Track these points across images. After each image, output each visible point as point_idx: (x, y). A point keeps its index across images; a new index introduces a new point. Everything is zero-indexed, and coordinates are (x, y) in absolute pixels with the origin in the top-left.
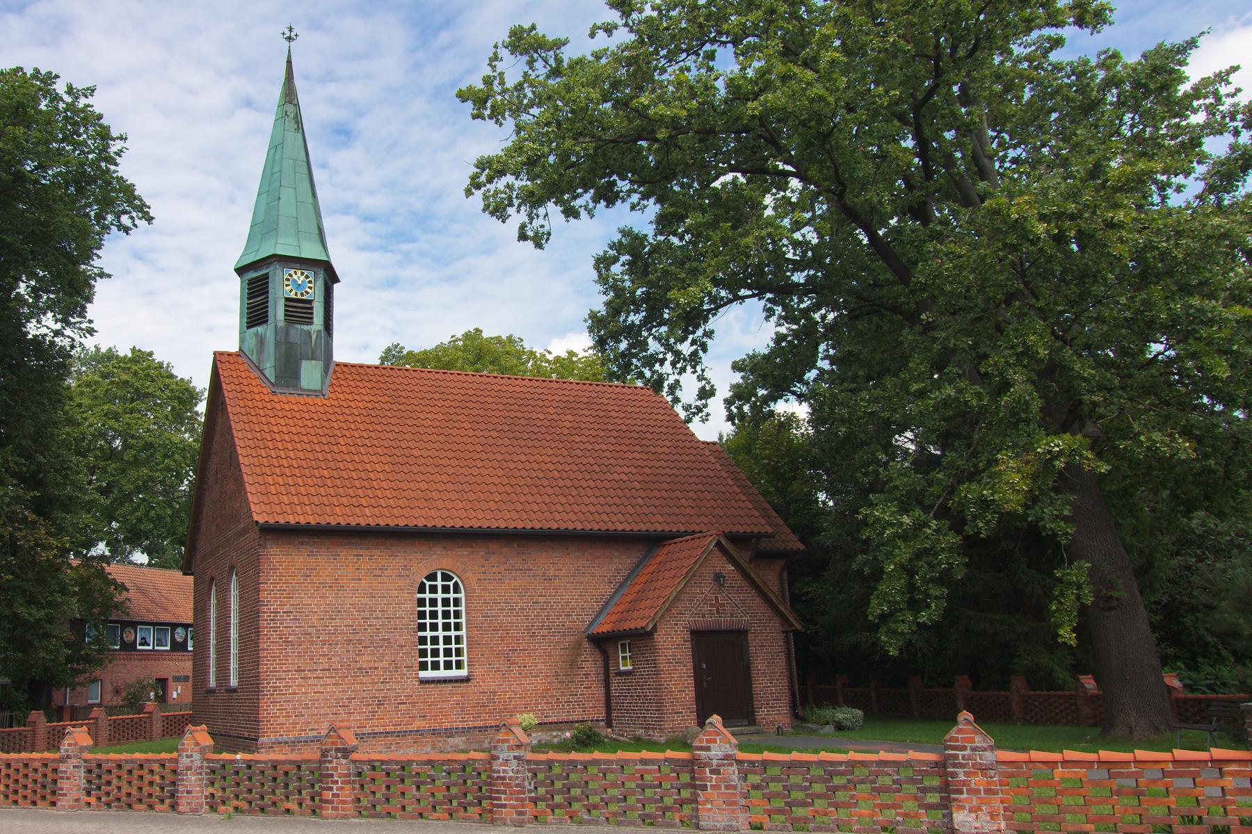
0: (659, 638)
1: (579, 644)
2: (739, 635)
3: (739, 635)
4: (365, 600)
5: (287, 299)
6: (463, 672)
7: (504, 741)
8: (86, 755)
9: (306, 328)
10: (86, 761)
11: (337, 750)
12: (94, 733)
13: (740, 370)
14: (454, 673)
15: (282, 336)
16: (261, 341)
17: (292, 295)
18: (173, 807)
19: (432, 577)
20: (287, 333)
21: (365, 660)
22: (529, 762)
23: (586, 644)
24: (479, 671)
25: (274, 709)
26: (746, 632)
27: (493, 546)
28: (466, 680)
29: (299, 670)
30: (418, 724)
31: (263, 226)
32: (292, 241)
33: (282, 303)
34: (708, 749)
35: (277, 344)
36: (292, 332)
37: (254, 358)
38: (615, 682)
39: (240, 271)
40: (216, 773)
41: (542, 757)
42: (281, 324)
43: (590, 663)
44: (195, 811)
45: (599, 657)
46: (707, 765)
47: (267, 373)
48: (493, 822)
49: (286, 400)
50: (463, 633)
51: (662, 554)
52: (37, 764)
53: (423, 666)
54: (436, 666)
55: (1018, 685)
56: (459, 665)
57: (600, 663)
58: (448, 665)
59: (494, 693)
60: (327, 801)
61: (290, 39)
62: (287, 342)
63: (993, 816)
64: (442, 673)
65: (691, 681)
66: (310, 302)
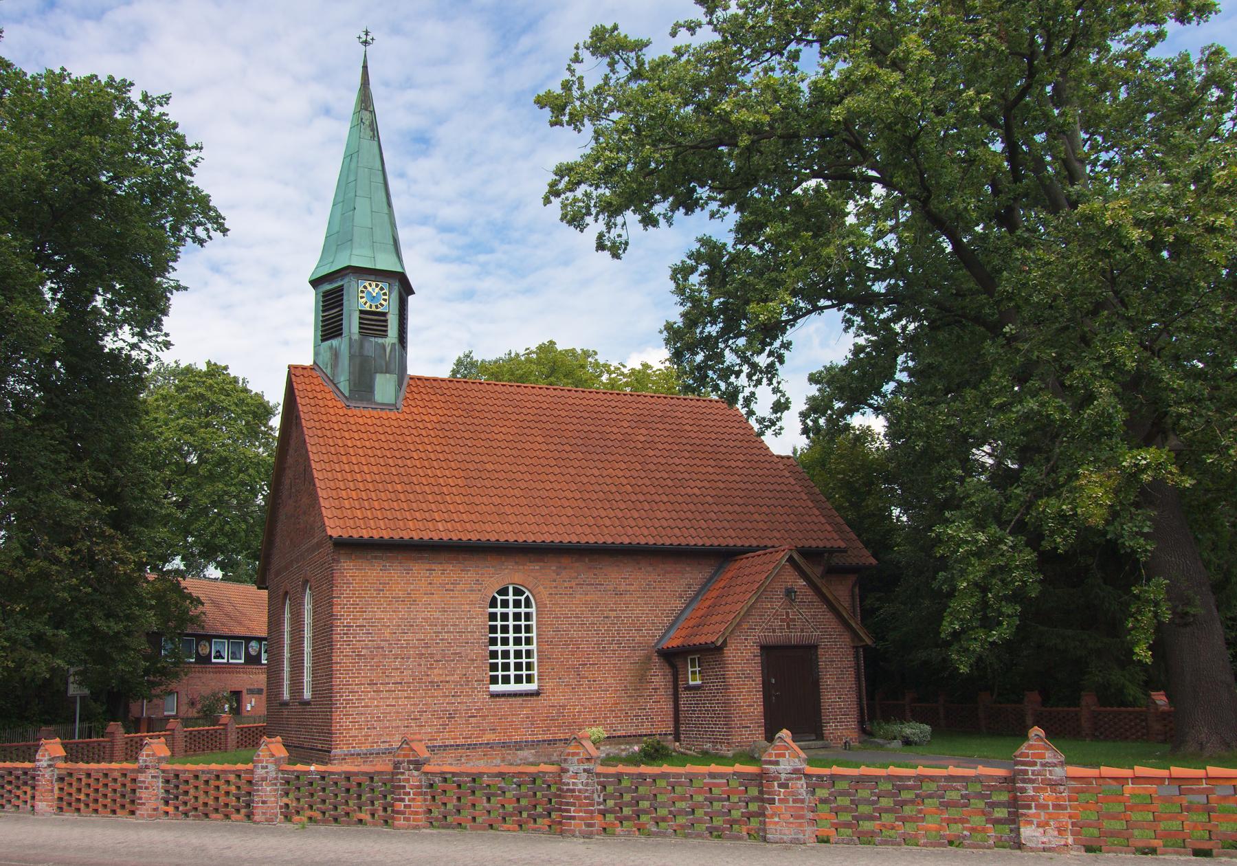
0: (729, 652)
1: (649, 658)
2: (810, 650)
3: (810, 650)
4: (437, 615)
5: (362, 312)
6: (533, 686)
7: (574, 754)
8: (164, 766)
9: (380, 340)
10: (163, 771)
11: (409, 762)
12: (171, 745)
13: (817, 382)
14: (524, 687)
15: (356, 348)
16: (336, 354)
17: (367, 308)
18: (249, 816)
19: (504, 591)
20: (361, 346)
21: (436, 674)
22: (598, 775)
23: (656, 659)
24: (549, 685)
25: (347, 722)
26: (815, 647)
27: (565, 561)
28: (536, 694)
29: (372, 684)
30: (489, 737)
31: (337, 238)
32: (367, 252)
33: (356, 315)
34: (777, 763)
35: (352, 357)
36: (366, 345)
37: (328, 372)
38: (683, 695)
39: (315, 283)
40: (290, 784)
41: (612, 770)
42: (356, 336)
43: (659, 678)
44: (269, 820)
45: (668, 671)
46: (776, 778)
47: (341, 386)
48: (562, 833)
49: (361, 414)
50: (534, 647)
51: (733, 568)
52: (117, 774)
53: (494, 680)
54: (506, 680)
55: (1088, 701)
56: (529, 679)
57: (669, 678)
58: (518, 679)
59: (564, 706)
60: (398, 812)
61: (366, 43)
62: (361, 355)
63: (1061, 831)
64: (513, 687)
65: (760, 695)
66: (384, 314)
